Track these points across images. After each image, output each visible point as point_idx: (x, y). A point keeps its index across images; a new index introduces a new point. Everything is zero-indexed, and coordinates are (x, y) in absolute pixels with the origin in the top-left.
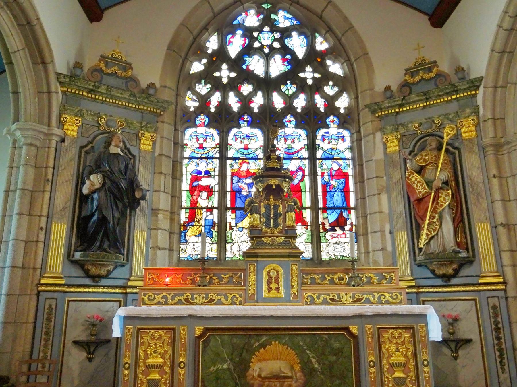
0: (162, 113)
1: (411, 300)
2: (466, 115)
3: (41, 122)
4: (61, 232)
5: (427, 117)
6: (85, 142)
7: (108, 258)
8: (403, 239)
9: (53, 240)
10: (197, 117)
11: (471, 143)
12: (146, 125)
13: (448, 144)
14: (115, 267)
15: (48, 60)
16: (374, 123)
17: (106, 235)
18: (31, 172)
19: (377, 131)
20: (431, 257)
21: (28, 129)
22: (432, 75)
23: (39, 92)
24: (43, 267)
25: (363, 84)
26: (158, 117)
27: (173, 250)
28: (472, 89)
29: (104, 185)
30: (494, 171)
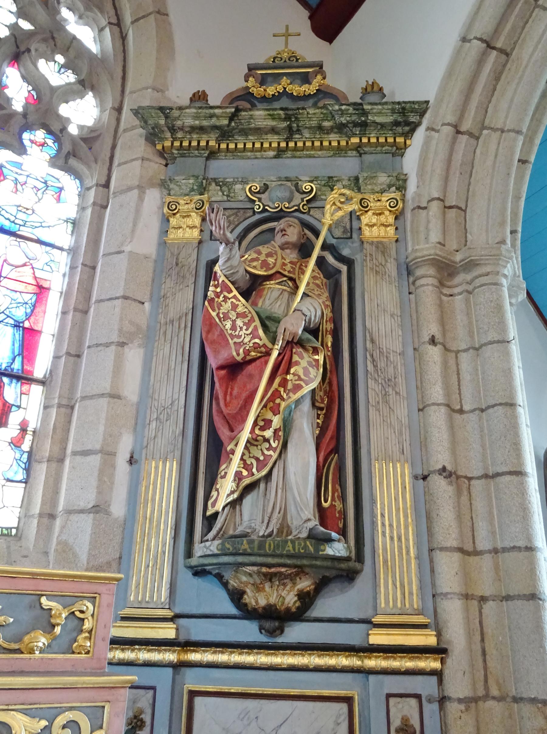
1: (153, 688)
2: (377, 189)
5: (284, 175)
8: (165, 482)
11: (383, 253)
13: (325, 247)
16: (146, 163)
19: (152, 185)
20: (239, 546)
22: (311, 89)
25: (141, 74)
28: (399, 129)
30: (432, 328)
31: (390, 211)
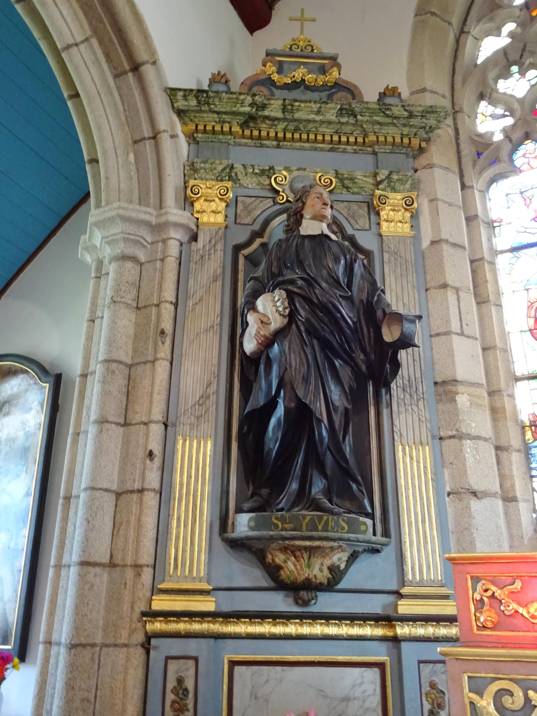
0: (424, 145)
3: (142, 201)
4: (199, 460)
6: (242, 237)
7: (325, 529)
9: (181, 485)
10: (515, 149)
12: (389, 177)
14: (353, 557)
15: (142, 55)
17: (314, 460)
18: (127, 320)
21: (111, 220)
23: (136, 142)
24: (158, 564)
26: (415, 157)
27: (514, 499)
29: (292, 316)
31: (220, 199)
